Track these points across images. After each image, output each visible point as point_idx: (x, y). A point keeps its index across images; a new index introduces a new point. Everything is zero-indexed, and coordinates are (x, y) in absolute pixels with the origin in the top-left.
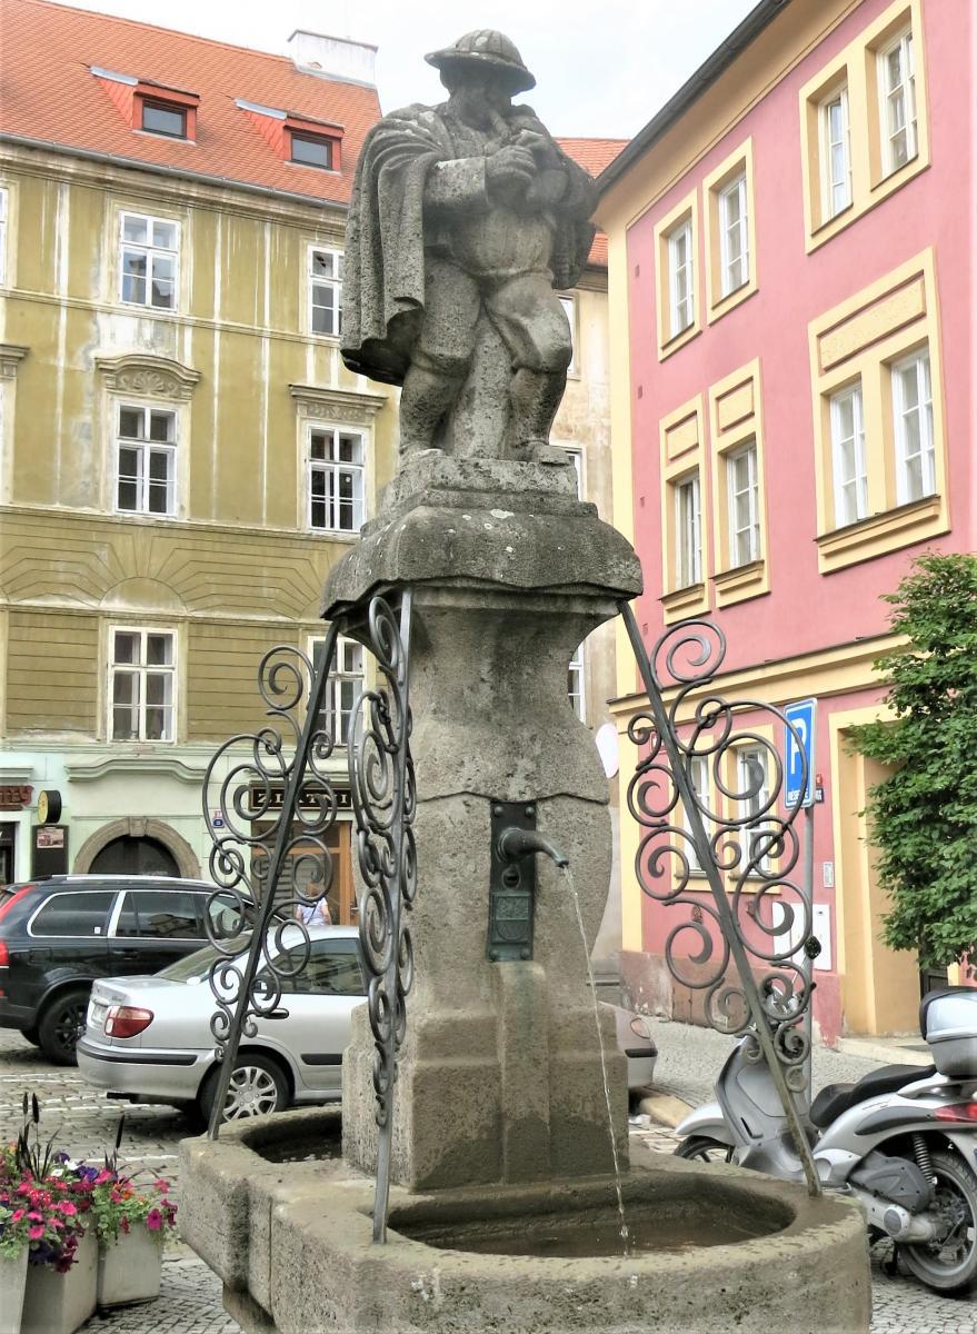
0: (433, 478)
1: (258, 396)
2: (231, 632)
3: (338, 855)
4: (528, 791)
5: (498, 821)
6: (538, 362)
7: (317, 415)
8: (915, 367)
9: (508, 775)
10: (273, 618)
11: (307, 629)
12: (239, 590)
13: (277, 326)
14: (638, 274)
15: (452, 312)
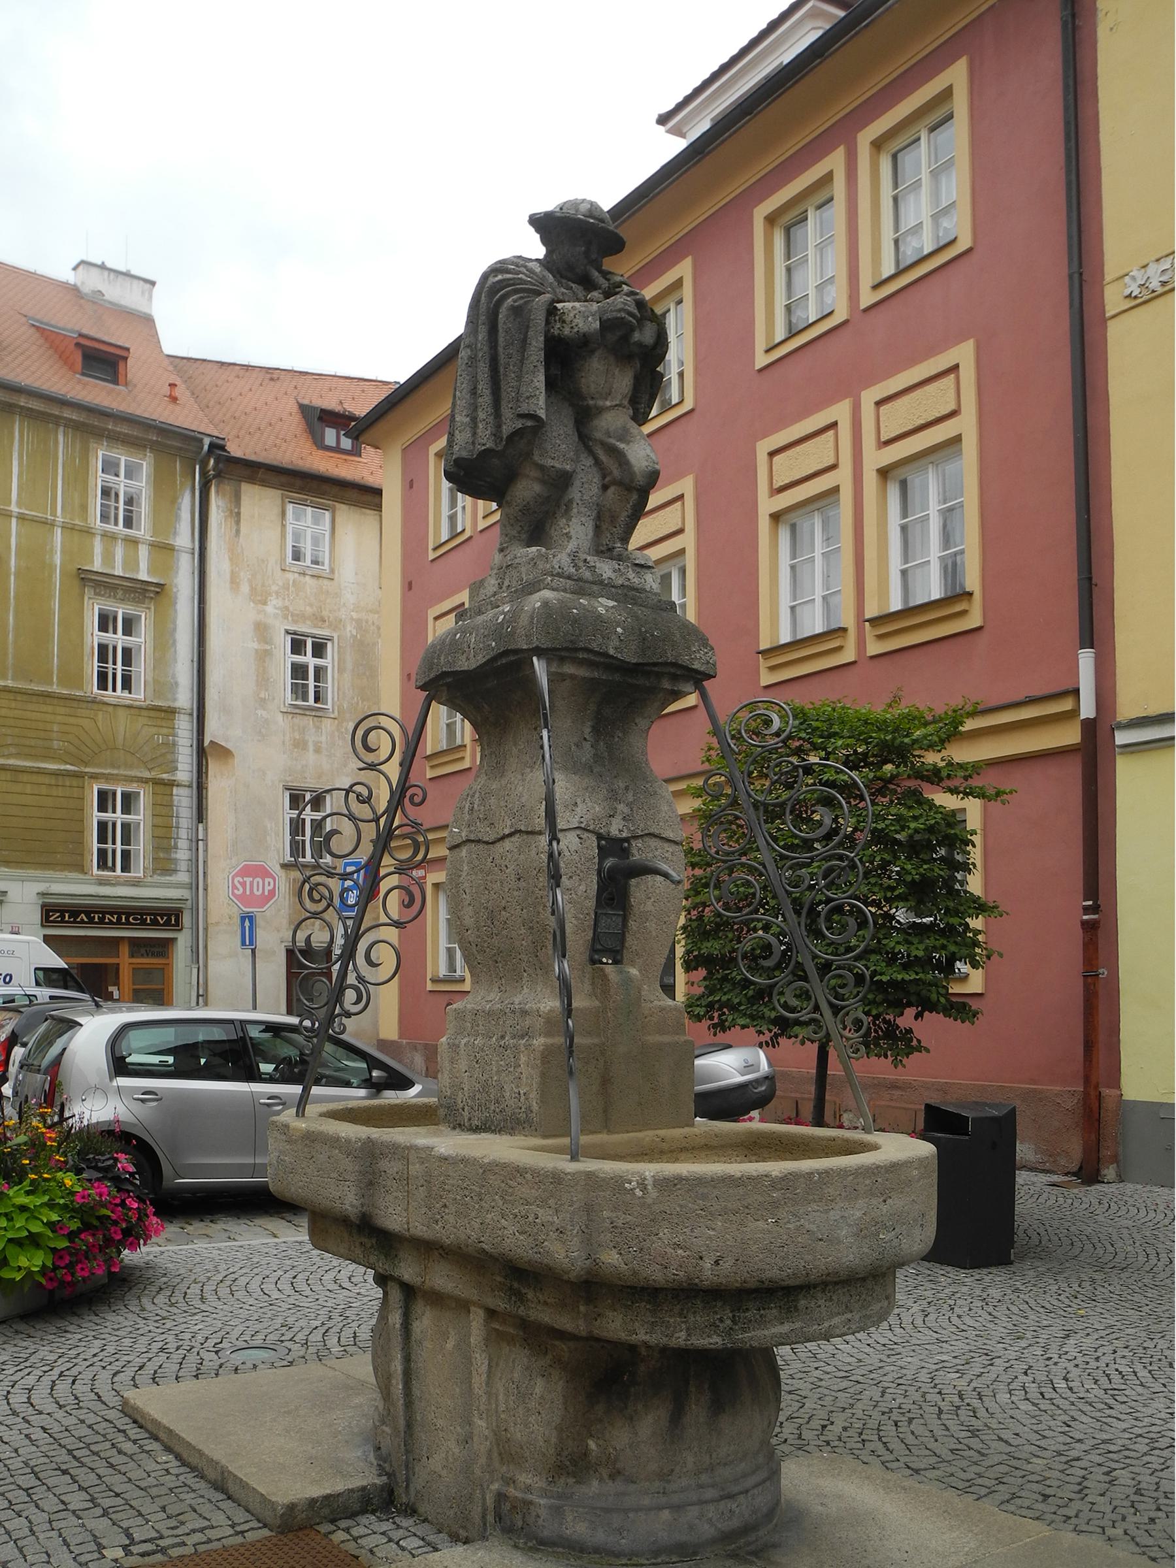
0: (553, 567)
1: (50, 576)
2: (25, 777)
3: (118, 964)
5: (603, 853)
6: (632, 481)
7: (103, 596)
8: (671, 573)
10: (63, 767)
11: (91, 777)
12: (33, 743)
13: (68, 516)
14: (411, 487)
15: (561, 432)
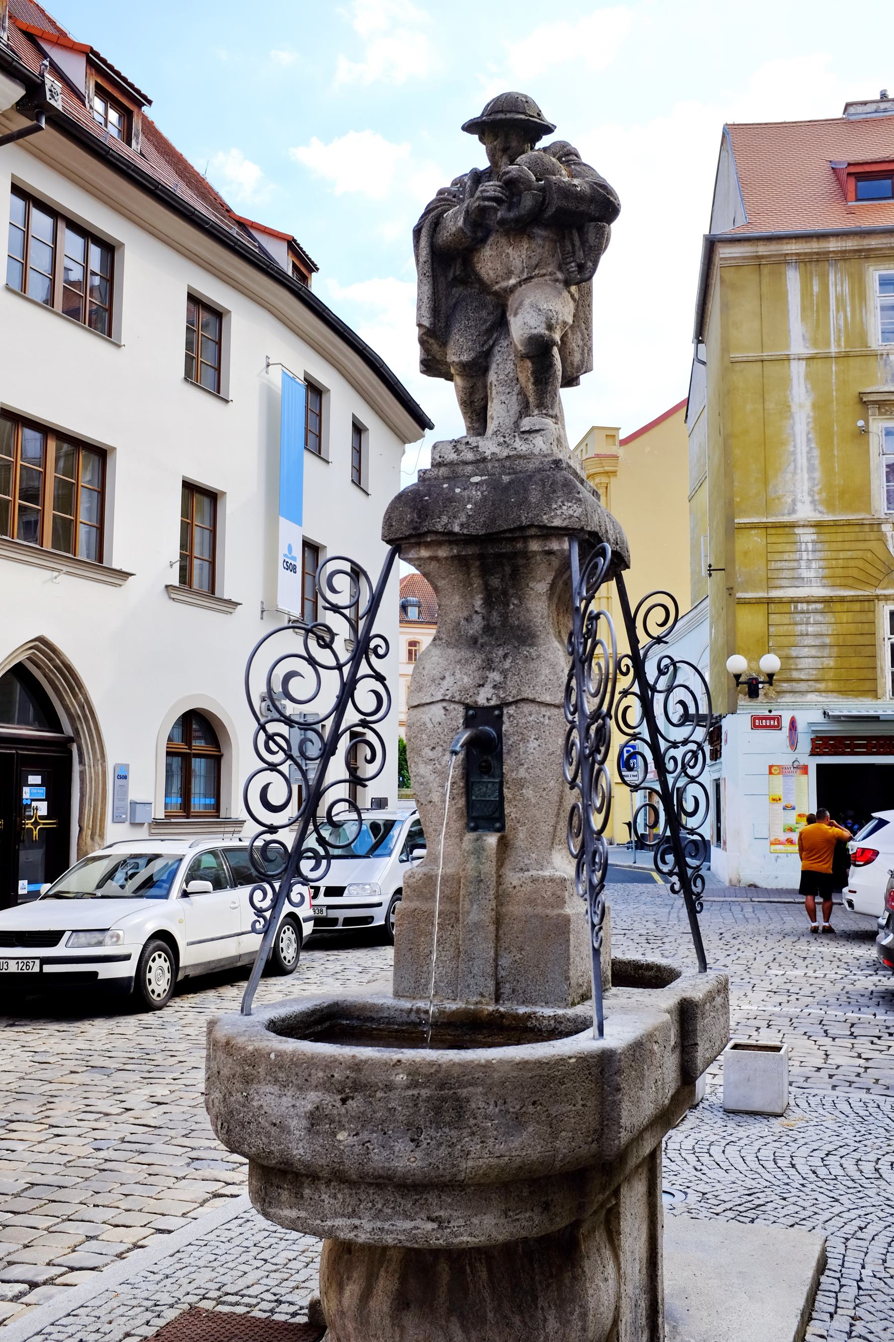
4: (494, 698)
5: (469, 722)
9: (480, 686)
